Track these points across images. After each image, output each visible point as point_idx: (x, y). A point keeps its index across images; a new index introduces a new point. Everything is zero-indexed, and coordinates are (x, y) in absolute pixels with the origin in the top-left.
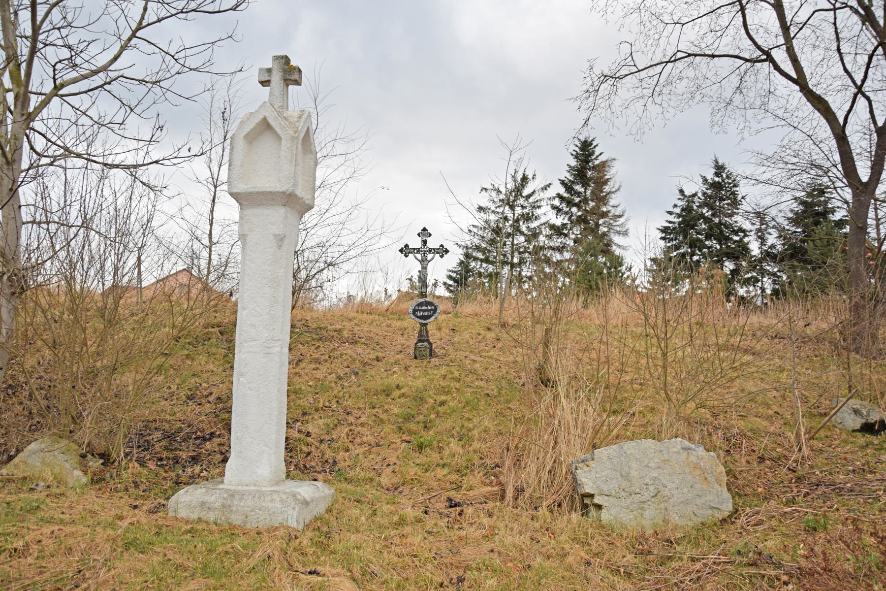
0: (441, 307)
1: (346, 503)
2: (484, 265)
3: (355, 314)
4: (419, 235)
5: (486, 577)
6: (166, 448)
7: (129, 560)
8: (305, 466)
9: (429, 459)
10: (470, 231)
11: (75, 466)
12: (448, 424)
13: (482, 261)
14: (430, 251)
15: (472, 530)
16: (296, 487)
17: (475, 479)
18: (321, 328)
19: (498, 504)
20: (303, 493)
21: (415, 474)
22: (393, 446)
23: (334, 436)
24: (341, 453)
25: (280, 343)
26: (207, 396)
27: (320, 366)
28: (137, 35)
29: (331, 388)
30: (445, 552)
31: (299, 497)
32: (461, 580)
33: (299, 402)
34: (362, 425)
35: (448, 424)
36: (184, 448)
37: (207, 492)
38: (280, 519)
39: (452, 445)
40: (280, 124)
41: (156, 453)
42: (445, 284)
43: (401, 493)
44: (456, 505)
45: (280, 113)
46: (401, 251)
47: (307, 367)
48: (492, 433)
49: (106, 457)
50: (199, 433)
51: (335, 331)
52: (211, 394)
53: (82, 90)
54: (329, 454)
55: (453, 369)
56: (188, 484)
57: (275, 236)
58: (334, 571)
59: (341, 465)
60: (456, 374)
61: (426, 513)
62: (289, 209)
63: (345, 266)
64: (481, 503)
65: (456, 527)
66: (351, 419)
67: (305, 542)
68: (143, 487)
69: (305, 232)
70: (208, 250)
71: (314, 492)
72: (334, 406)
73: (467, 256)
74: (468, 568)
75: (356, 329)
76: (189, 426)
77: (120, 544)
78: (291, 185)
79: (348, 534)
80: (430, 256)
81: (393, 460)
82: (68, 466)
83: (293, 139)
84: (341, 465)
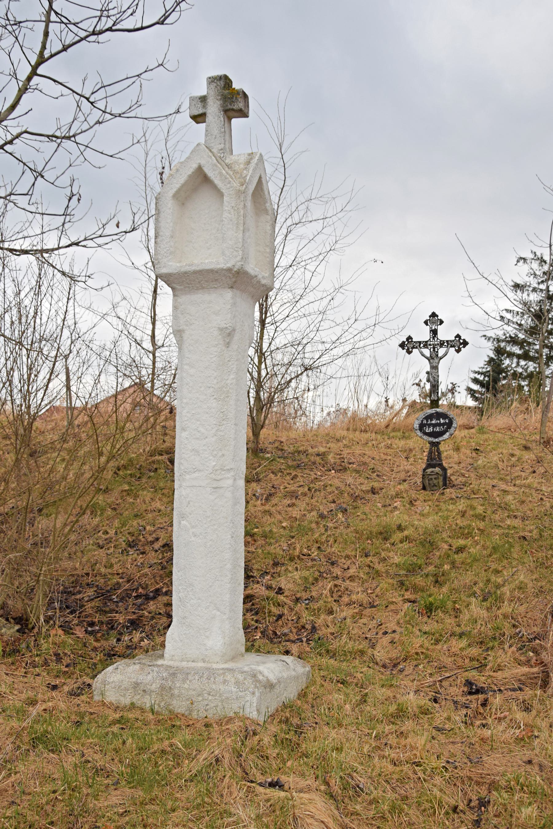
0: (458, 421)
1: (326, 684)
2: (523, 363)
3: (345, 433)
4: (426, 323)
5: (521, 802)
6: (100, 611)
7: (35, 761)
8: (275, 633)
9: (441, 626)
10: (502, 318)
12: (468, 578)
13: (519, 357)
14: (442, 344)
15: (501, 728)
16: (258, 664)
17: (505, 655)
18: (299, 452)
19: (539, 692)
20: (266, 673)
21: (421, 646)
22: (392, 607)
23: (314, 594)
24: (322, 617)
25: (232, 473)
26: (152, 543)
27: (297, 502)
28: (39, 71)
29: (311, 530)
30: (460, 760)
31: (261, 678)
32: (483, 803)
33: (268, 548)
34: (352, 578)
35: (468, 578)
36: (122, 609)
37: (142, 669)
38: (235, 707)
39: (473, 607)
40: (220, 174)
41: (86, 616)
42: (469, 390)
43: (401, 671)
44: (477, 692)
45: (220, 160)
46: (402, 345)
47: (280, 502)
48: (530, 589)
50: (140, 590)
51: (318, 455)
52: (157, 539)
54: (306, 617)
55: (475, 503)
56: (123, 656)
57: (221, 330)
58: (303, 783)
59: (321, 632)
60: (480, 510)
61: (435, 701)
62: (238, 293)
63: (330, 370)
64: (514, 690)
65: (478, 723)
66: (337, 571)
67: (266, 740)
68: (66, 660)
69: (273, 327)
70: (151, 356)
71: (282, 671)
72: (315, 554)
73: (499, 351)
74: (493, 786)
75: (346, 452)
76: (128, 581)
77: (26, 739)
78: (239, 258)
79: (326, 729)
80: (441, 351)
81: (391, 626)
83: (240, 193)
84: (321, 632)
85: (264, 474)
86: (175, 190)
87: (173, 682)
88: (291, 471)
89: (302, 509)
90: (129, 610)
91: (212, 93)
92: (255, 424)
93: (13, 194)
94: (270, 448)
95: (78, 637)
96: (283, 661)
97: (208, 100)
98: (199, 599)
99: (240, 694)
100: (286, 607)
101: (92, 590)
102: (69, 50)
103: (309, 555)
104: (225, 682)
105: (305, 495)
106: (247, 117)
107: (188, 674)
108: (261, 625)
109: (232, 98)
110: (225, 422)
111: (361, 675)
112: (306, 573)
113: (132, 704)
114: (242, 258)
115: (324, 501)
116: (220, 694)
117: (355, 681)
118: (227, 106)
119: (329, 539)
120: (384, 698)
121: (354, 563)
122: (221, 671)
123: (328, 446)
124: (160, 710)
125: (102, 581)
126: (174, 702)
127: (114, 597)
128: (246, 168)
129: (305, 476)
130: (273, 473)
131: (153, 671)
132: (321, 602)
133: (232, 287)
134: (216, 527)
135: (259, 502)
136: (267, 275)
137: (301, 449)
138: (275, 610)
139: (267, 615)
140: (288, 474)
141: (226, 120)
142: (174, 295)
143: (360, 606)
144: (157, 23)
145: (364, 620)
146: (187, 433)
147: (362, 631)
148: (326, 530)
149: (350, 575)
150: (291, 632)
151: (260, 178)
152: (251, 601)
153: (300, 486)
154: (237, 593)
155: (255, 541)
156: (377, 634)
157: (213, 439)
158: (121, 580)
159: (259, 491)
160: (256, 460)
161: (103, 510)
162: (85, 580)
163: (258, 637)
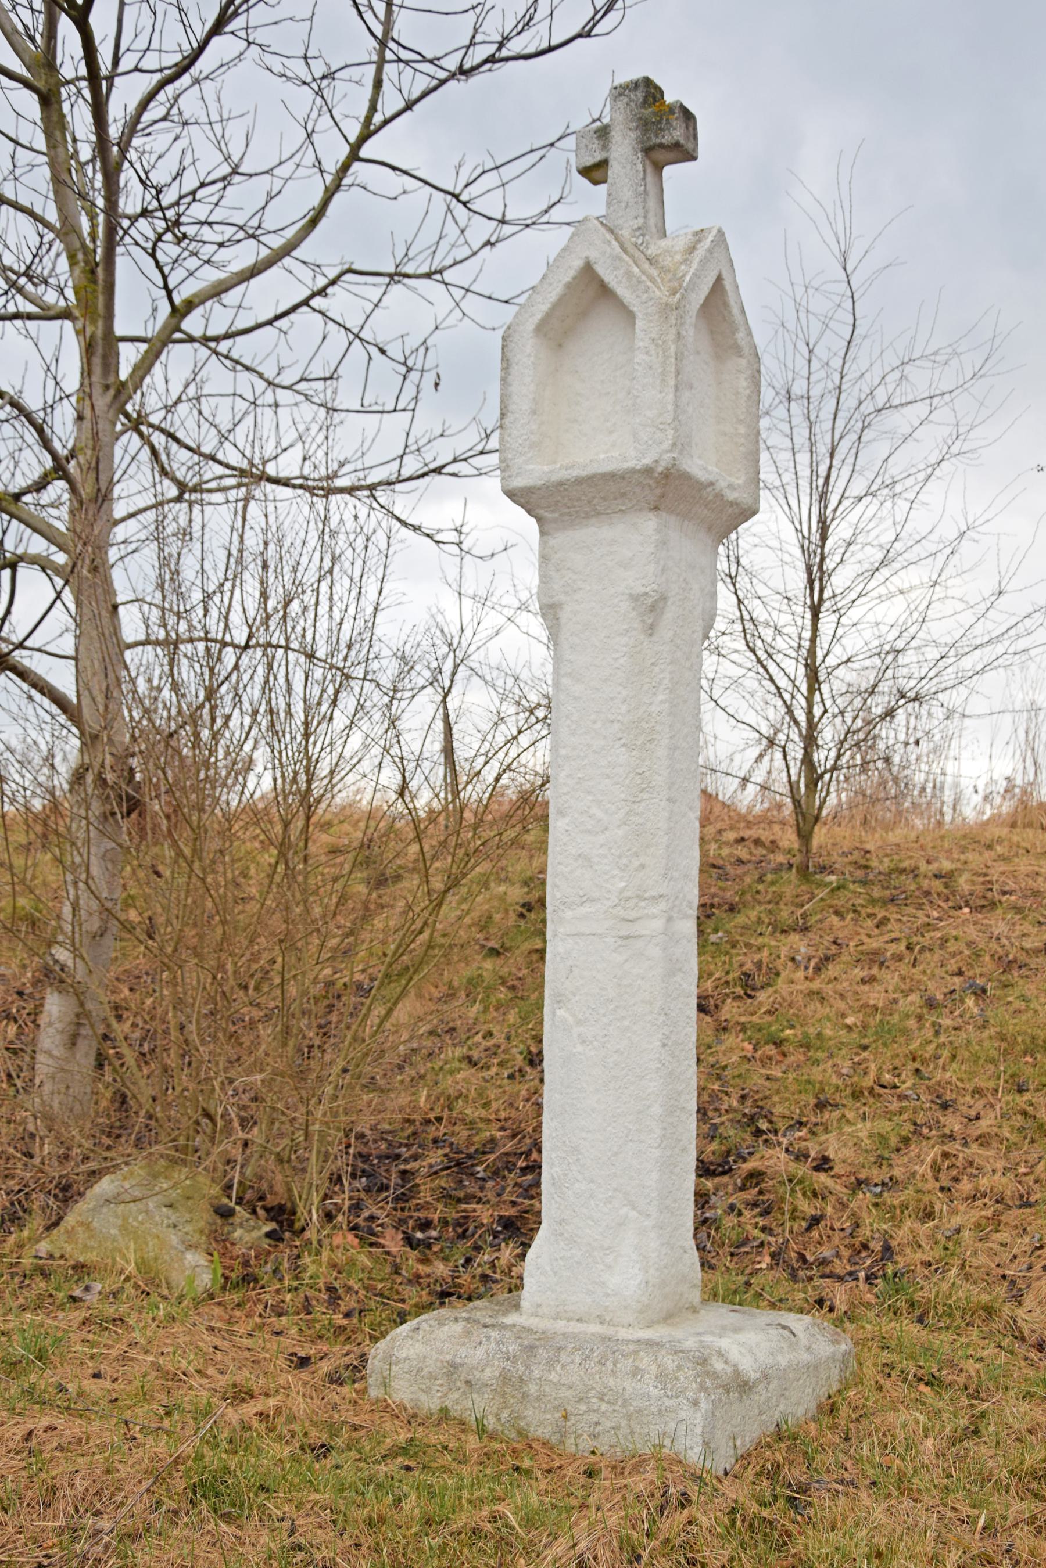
6: (446, 1197)
8: (802, 1258)
11: (196, 1238)
20: (735, 1354)
23: (897, 1172)
25: (663, 905)
27: (883, 974)
28: (363, 153)
29: (905, 1032)
31: (719, 1366)
34: (983, 1140)
36: (491, 1195)
37: (468, 1333)
40: (629, 274)
47: (845, 974)
49: (283, 1218)
53: (261, 320)
54: (873, 1225)
57: (635, 598)
66: (953, 1123)
68: (349, 1302)
71: (778, 1352)
72: (908, 1083)
77: (179, 1485)
78: (666, 445)
82: (174, 1239)
85: (819, 917)
86: (539, 317)
87: (527, 1367)
88: (876, 910)
89: (891, 988)
90: (505, 1197)
91: (620, 117)
92: (803, 815)
93: (306, 380)
94: (839, 862)
95: (388, 1253)
96: (784, 1327)
97: (613, 133)
98: (592, 1181)
99: (668, 1402)
100: (832, 1199)
101: (440, 1152)
102: (416, 108)
103: (895, 1087)
104: (636, 1372)
105: (899, 958)
106: (694, 158)
107: (559, 1349)
108: (772, 1239)
109: (660, 122)
110: (645, 796)
111: (977, 1366)
112: (884, 1126)
113: (445, 1412)
114: (674, 444)
115: (939, 972)
116: (625, 1401)
117: (961, 1380)
118: (649, 139)
119: (940, 1052)
120: (1024, 1426)
121: (992, 1106)
122: (632, 1347)
123: (963, 857)
124: (500, 1428)
125: (465, 1133)
126: (529, 1412)
127: (478, 1169)
128: (686, 260)
129: (904, 919)
130: (837, 913)
131: (488, 1338)
132: (910, 1191)
133: (656, 508)
134: (626, 1023)
135: (800, 974)
136: (740, 482)
137: (905, 864)
138: (807, 1207)
139: (787, 1216)
140: (869, 916)
141: (649, 169)
142: (542, 533)
143: (997, 1202)
144: (579, 36)
145: (1003, 1236)
146: (567, 820)
147: (997, 1260)
148: (937, 1033)
149: (979, 1132)
150: (838, 1255)
151: (719, 279)
152: (757, 1184)
153: (892, 941)
154: (677, 1170)
155: (784, 1055)
156: (1030, 1268)
157: (620, 832)
158: (499, 1134)
159: (803, 950)
160: (804, 888)
161: (489, 990)
162: (432, 1131)
163: (764, 1266)
